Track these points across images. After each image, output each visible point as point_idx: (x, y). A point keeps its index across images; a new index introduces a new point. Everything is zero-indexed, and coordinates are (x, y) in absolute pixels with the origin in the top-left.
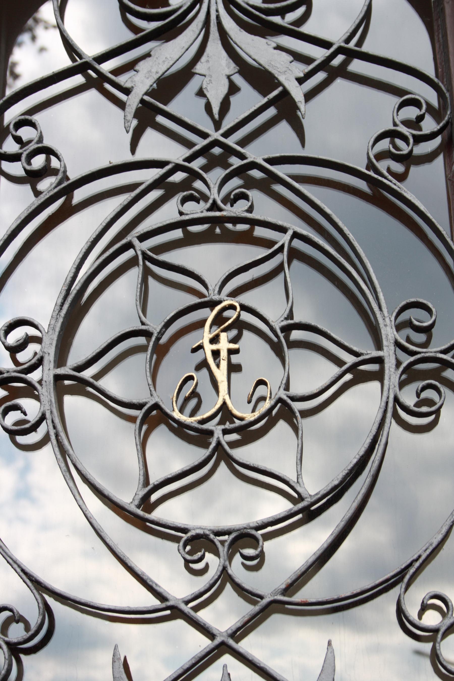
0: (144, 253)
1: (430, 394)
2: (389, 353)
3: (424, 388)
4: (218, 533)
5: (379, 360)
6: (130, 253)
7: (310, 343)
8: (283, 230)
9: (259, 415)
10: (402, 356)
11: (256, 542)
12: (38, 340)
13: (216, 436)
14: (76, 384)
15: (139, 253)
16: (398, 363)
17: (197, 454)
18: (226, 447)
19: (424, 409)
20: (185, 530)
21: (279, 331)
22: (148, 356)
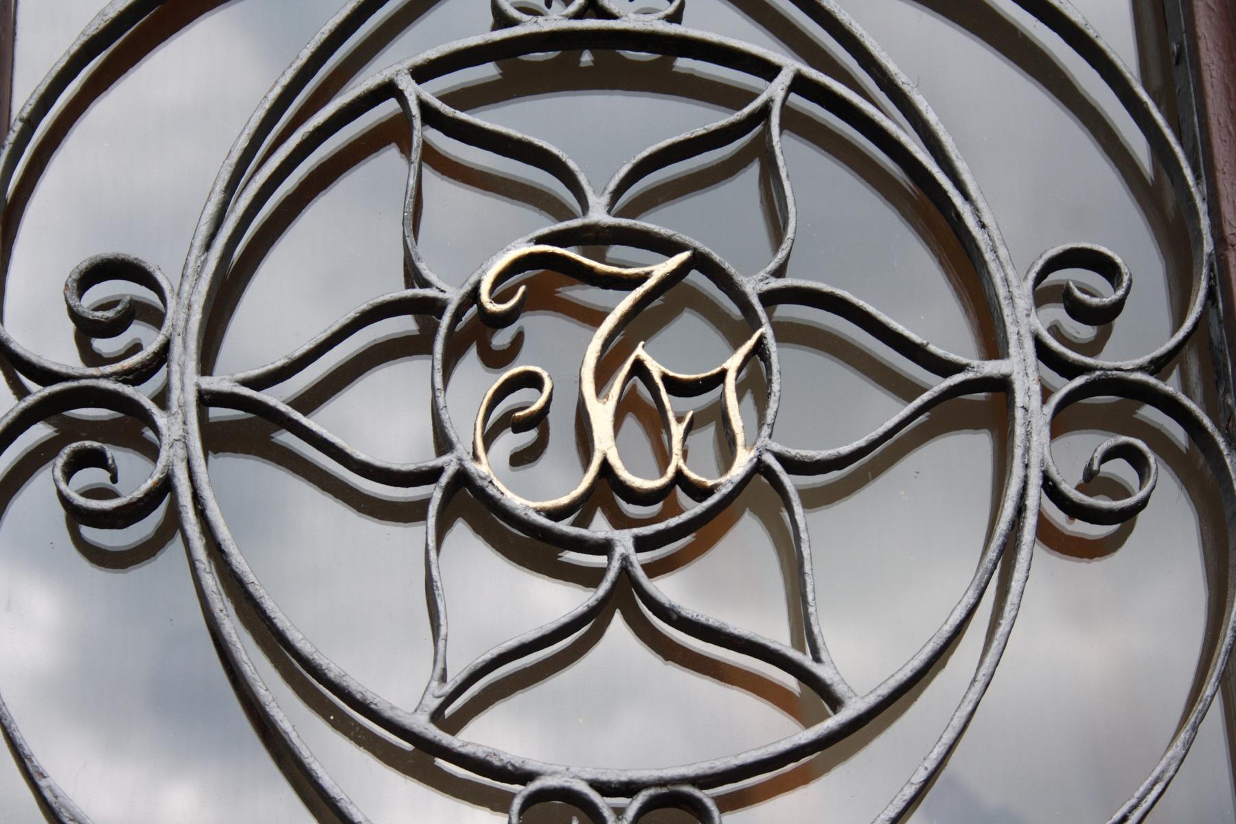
0: (423, 105)
1: (1120, 469)
2: (1020, 367)
3: (1109, 455)
4: (605, 789)
5: (1002, 386)
6: (389, 107)
7: (836, 337)
8: (769, 71)
9: (1219, 167)
10: (1052, 377)
11: (756, 421)
12: (155, 318)
13: (619, 551)
14: (1119, 529)
15: (415, 110)
16: (1046, 393)
17: (561, 601)
18: (640, 574)
19: (1104, 503)
20: (525, 777)
21: (755, 301)
22: (438, 365)
